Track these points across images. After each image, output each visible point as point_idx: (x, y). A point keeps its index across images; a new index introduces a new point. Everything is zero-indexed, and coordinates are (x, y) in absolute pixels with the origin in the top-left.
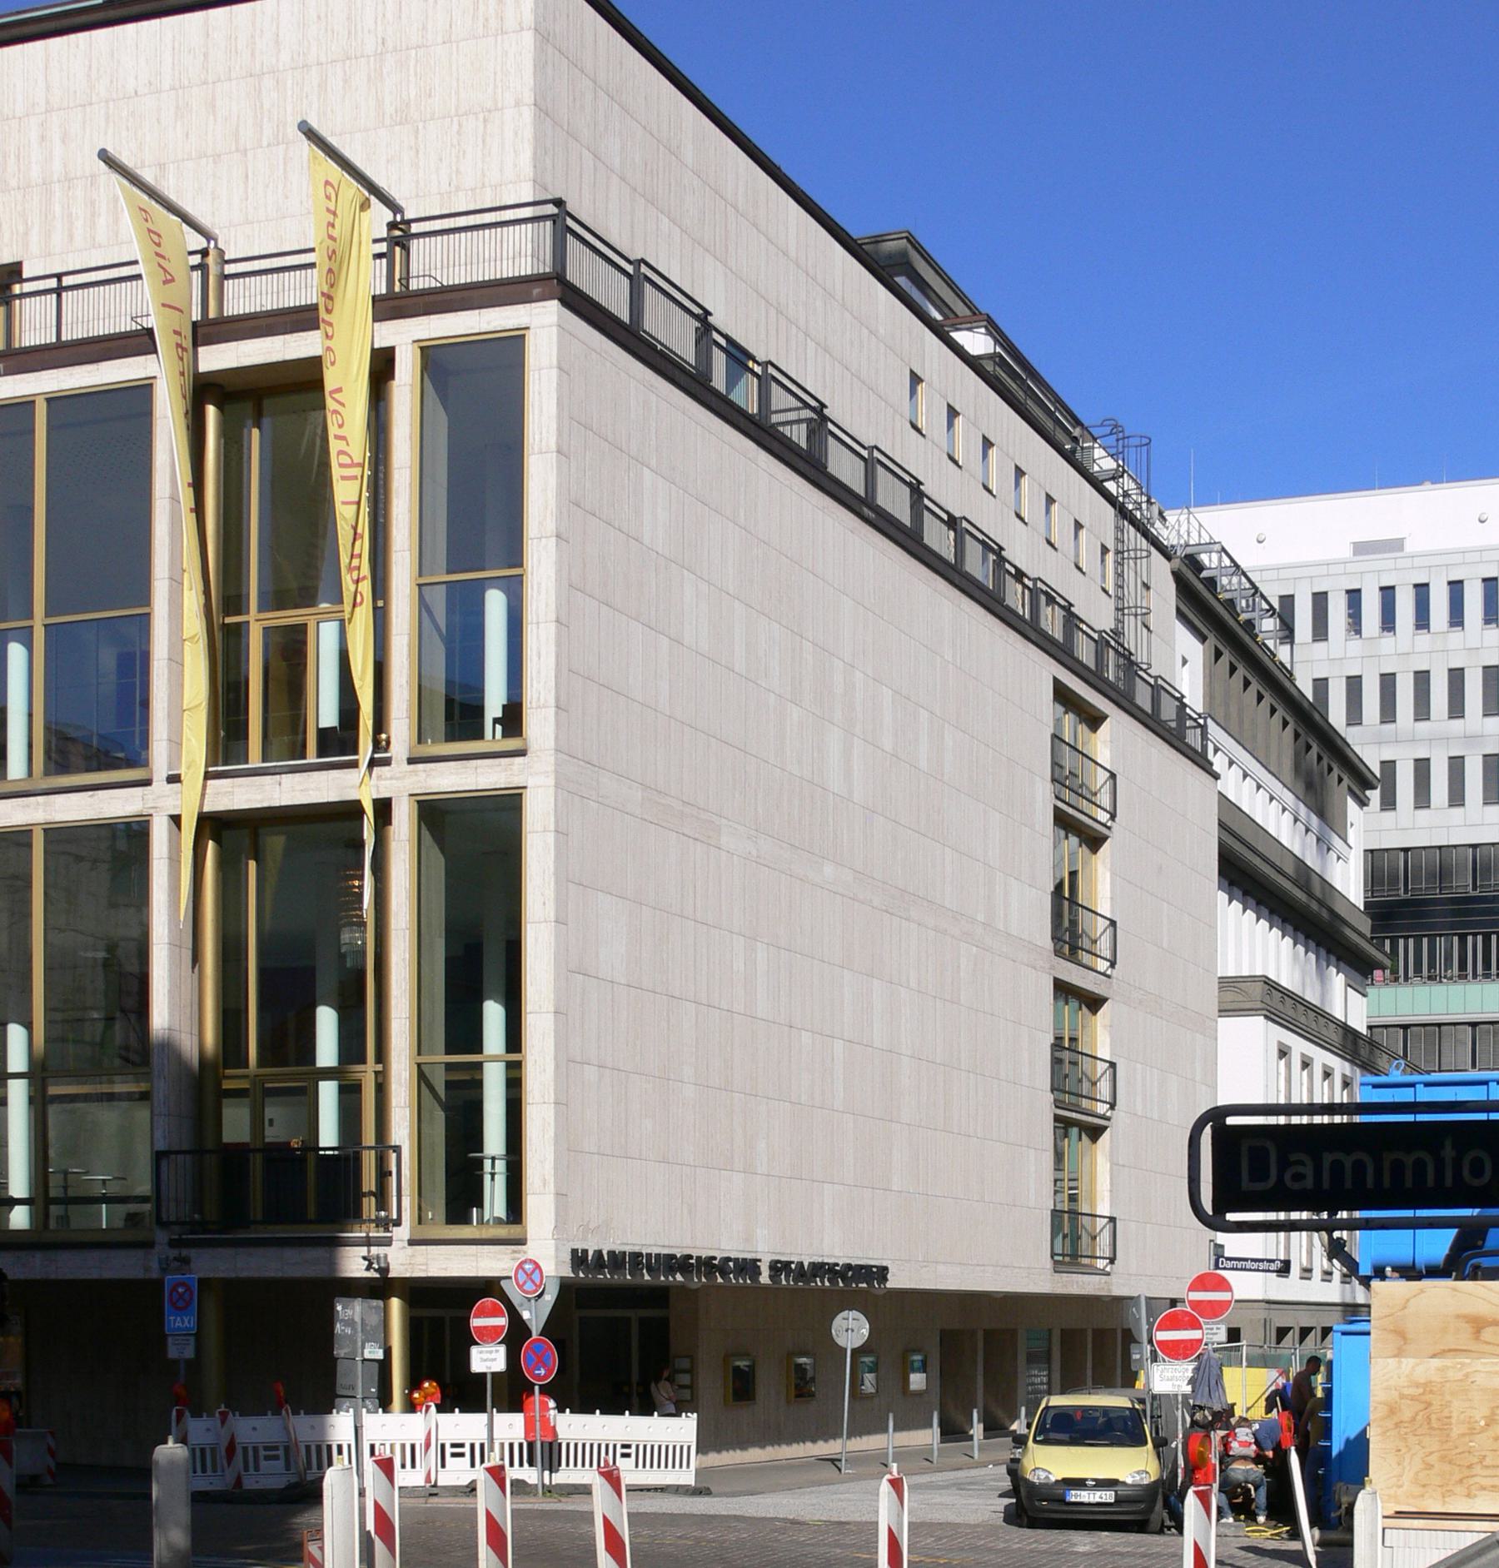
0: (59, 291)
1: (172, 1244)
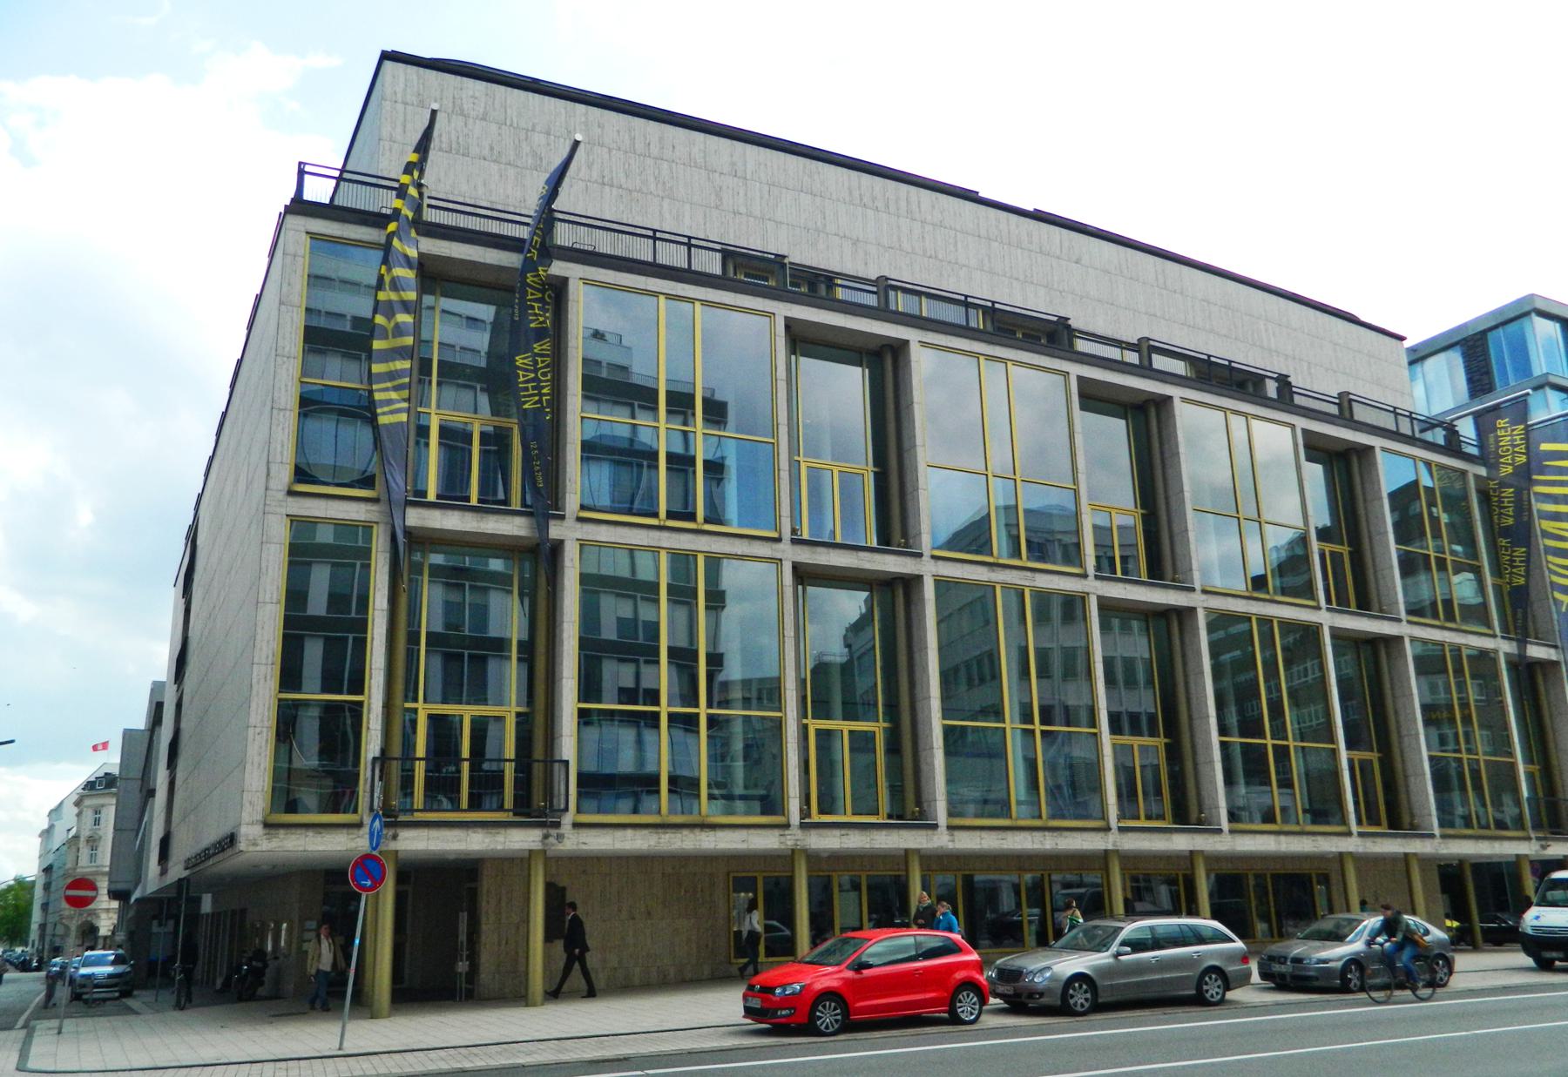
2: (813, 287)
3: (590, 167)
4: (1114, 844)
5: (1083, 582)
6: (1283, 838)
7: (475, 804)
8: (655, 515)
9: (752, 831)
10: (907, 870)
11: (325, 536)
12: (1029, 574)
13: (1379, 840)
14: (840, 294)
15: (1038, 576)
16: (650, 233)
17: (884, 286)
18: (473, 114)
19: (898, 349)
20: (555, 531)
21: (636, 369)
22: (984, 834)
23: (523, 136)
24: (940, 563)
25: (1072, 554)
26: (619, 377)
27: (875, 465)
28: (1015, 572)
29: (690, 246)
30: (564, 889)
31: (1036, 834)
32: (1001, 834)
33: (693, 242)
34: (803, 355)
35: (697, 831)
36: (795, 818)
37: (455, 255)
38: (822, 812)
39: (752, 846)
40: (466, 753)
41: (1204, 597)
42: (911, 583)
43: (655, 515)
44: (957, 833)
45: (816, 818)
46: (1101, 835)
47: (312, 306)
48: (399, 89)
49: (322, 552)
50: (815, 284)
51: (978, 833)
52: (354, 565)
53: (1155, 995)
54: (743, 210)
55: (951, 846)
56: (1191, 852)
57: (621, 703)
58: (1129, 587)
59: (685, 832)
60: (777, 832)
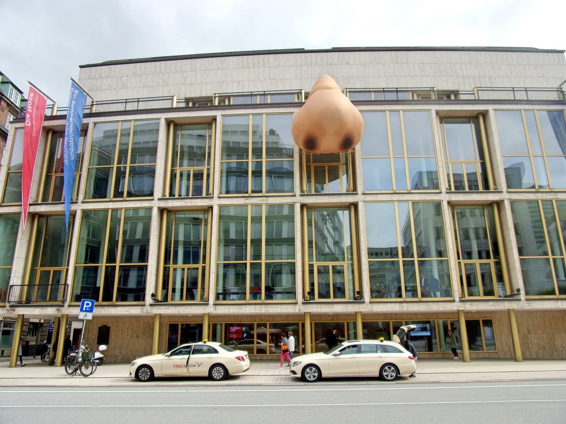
0: (138, 101)
1: (10, 306)
2: (449, 97)
3: (140, 83)
4: (299, 310)
5: (294, 198)
6: (405, 304)
7: (51, 300)
8: (247, 193)
9: (130, 307)
10: (459, 318)
11: (232, 213)
12: (265, 198)
13: (499, 303)
14: (462, 97)
15: (269, 199)
16: (512, 89)
17: (223, 98)
18: (104, 77)
19: (484, 114)
20: (74, 207)
21: (281, 142)
22: (231, 307)
23: (119, 79)
24: (222, 199)
25: (434, 184)
26: (275, 146)
27: (481, 160)
28: (257, 199)
29: (514, 91)
30: (109, 328)
31: (257, 306)
32: (239, 307)
33: (515, 89)
34: (445, 123)
35: (110, 307)
36: (457, 299)
37: (55, 124)
38: (469, 295)
39: (130, 313)
40: (50, 283)
41: (363, 196)
42: (499, 204)
43: (247, 193)
44: (218, 307)
45: (467, 298)
46: (293, 306)
47: (268, 141)
48: (83, 76)
49: (232, 218)
50: (448, 96)
51: (228, 307)
52: (273, 222)
53: (553, 377)
54: (194, 82)
55: (214, 312)
56: (508, 310)
57: (139, 262)
58: (318, 197)
59: (106, 308)
60: (140, 308)
